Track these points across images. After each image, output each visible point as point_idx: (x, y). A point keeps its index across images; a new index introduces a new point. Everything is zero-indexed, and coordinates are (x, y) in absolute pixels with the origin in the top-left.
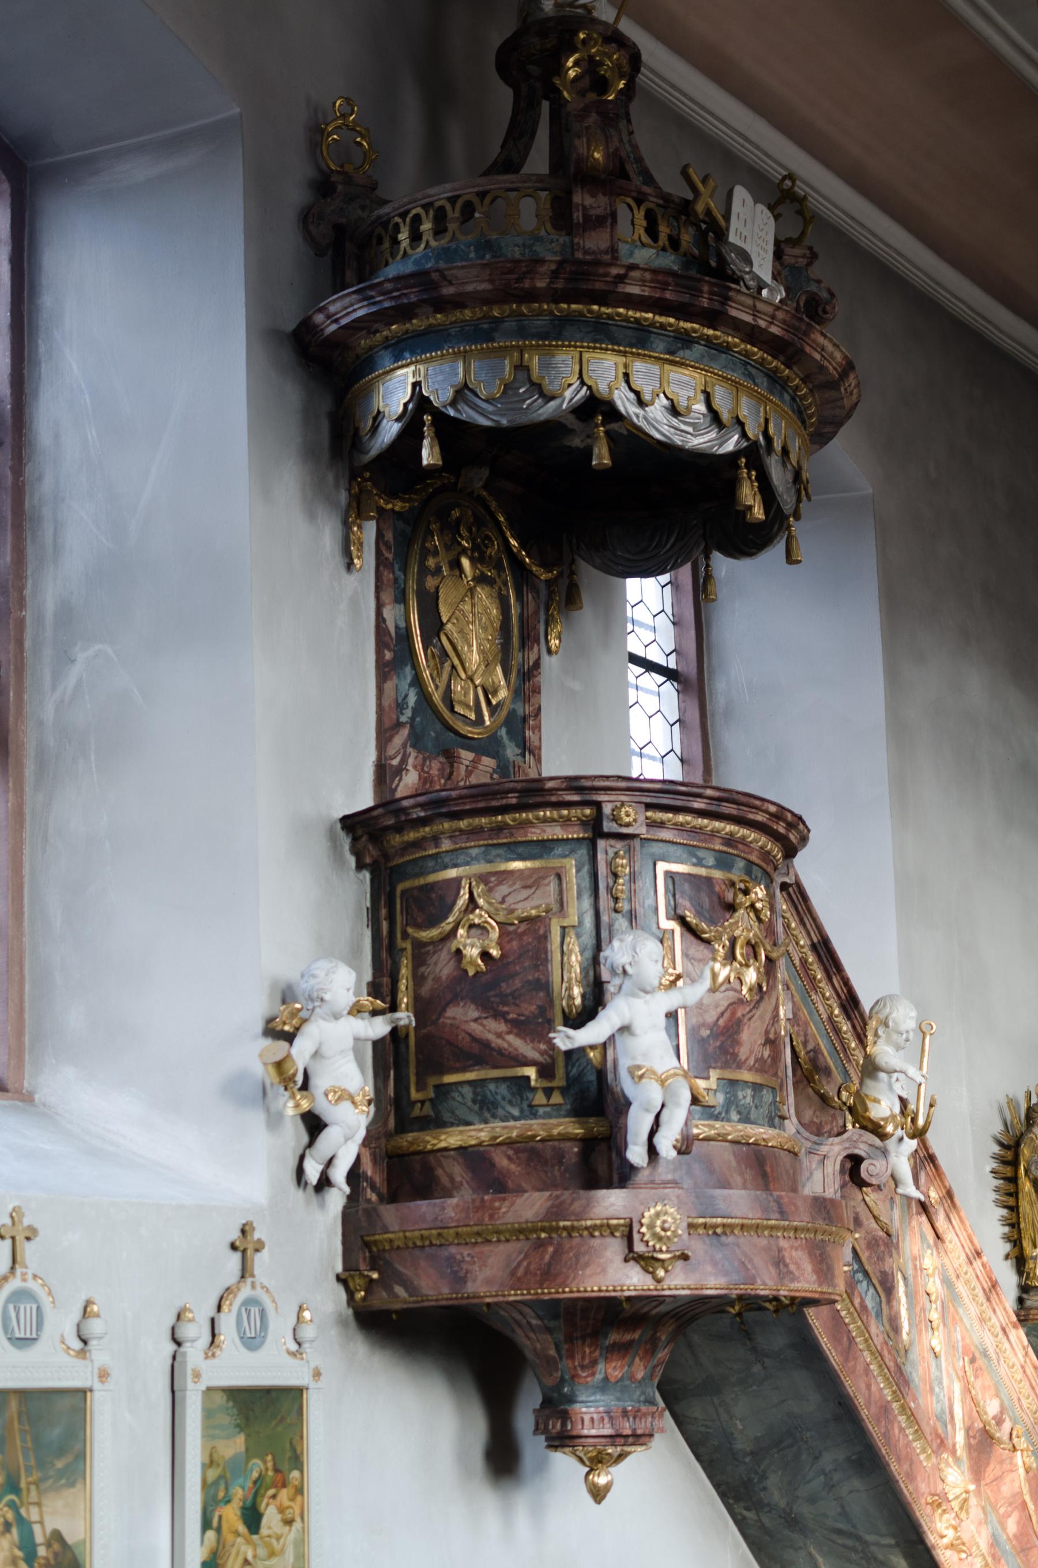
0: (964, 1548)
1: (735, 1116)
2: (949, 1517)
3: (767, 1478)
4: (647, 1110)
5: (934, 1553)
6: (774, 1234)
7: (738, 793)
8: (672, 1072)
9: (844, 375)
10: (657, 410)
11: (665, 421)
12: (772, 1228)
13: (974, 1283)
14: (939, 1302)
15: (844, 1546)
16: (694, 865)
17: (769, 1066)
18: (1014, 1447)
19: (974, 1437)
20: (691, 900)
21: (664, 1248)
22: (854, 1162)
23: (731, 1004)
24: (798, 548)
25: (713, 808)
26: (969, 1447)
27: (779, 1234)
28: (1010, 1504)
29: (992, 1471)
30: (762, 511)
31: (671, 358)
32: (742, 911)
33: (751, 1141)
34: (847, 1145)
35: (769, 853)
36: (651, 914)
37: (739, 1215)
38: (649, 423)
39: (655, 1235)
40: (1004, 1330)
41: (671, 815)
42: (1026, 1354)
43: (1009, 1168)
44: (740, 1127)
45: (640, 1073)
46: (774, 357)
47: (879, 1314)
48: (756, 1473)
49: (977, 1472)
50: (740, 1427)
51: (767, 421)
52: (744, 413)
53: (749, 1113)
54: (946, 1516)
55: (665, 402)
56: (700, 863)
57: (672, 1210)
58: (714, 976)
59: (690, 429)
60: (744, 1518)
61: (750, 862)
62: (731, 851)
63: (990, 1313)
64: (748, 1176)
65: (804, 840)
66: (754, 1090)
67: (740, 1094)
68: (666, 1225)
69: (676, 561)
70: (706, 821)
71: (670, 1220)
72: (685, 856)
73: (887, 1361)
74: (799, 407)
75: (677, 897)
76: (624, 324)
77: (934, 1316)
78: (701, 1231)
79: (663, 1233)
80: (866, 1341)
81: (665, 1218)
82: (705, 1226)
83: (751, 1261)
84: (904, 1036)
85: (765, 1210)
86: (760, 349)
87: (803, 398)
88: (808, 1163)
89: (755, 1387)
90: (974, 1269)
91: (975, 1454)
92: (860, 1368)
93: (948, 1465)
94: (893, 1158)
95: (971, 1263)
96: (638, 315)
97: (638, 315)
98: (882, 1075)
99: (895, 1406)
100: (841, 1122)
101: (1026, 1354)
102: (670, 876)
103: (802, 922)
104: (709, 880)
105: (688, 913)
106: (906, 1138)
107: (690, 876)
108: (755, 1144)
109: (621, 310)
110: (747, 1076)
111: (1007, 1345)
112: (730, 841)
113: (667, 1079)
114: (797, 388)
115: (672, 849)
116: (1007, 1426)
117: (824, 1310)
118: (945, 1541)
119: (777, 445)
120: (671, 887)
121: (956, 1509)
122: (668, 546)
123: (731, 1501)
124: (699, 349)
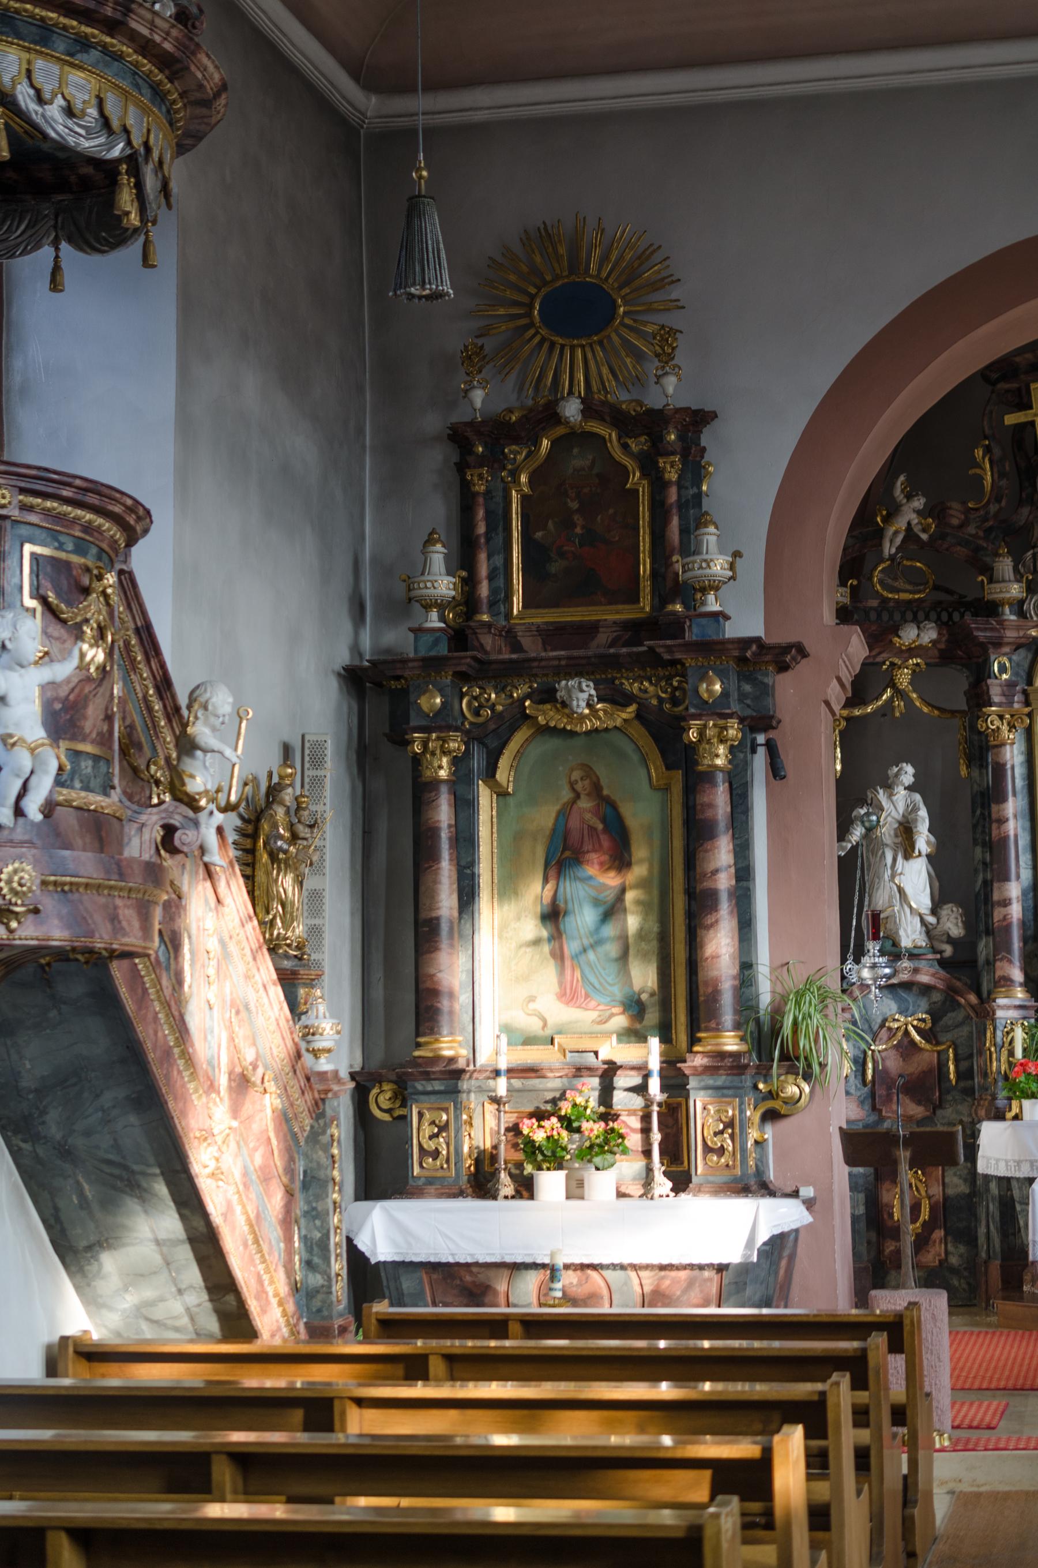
0: (222, 1177)
1: (78, 785)
2: (213, 1150)
3: (47, 1113)
4: (18, 776)
5: (196, 1181)
6: (112, 893)
7: (103, 485)
8: (40, 742)
9: (217, 95)
10: (55, 110)
11: (61, 121)
12: (111, 888)
13: (245, 944)
14: (215, 960)
15: (111, 1175)
16: (56, 549)
17: (104, 740)
18: (265, 1090)
19: (234, 1080)
20: (52, 581)
21: (19, 902)
22: (169, 830)
23: (80, 681)
24: (155, 253)
25: (80, 497)
26: (230, 1088)
27: (116, 893)
28: (258, 1140)
29: (248, 1108)
30: (138, 218)
31: (72, 60)
32: (95, 595)
33: (92, 807)
34: (164, 815)
35: (116, 542)
36: (16, 592)
37: (85, 874)
38: (47, 121)
39: (12, 890)
40: (265, 986)
41: (39, 500)
42: (281, 1008)
43: (249, 841)
44: (83, 794)
45: (12, 741)
46: (161, 71)
47: (168, 968)
48: (38, 1108)
49: (235, 1111)
50: (28, 1066)
51: (149, 131)
52: (130, 121)
53: (89, 782)
54: (210, 1149)
55: (62, 103)
56: (60, 547)
57: (29, 868)
58: (82, 655)
59: (82, 132)
60: (20, 1149)
61: (102, 550)
62: (88, 538)
63: (255, 971)
64: (88, 840)
65: (146, 531)
66: (94, 761)
67: (83, 764)
68: (23, 881)
69: (26, 248)
70: (70, 509)
71: (26, 876)
72: (49, 540)
73: (173, 1010)
74: (171, 119)
75: (40, 577)
76: (30, 20)
77: (211, 971)
78: (51, 888)
79: (19, 888)
80: (157, 992)
81: (22, 874)
82: (55, 883)
83: (91, 917)
84: (221, 719)
85: (108, 871)
86: (150, 62)
87: (177, 111)
88: (131, 829)
89: (48, 1031)
90: (245, 932)
91: (234, 1095)
92: (150, 1016)
93: (215, 1103)
94: (203, 828)
95: (243, 926)
96: (44, 13)
97: (44, 13)
98: (199, 753)
99: (176, 1051)
100: (148, 793)
101: (281, 1008)
102: (34, 556)
103: (129, 607)
104: (67, 564)
105: (50, 594)
106: (216, 812)
107: (52, 558)
108: (95, 811)
109: (28, 6)
110: (88, 748)
111: (265, 1000)
112: (88, 528)
113: (36, 748)
114: (174, 102)
115: (38, 532)
116: (260, 1071)
117: (125, 963)
118: (208, 1170)
119: (156, 155)
120: (35, 568)
121: (220, 1143)
122: (19, 232)
123: (9, 1134)
124: (95, 54)
